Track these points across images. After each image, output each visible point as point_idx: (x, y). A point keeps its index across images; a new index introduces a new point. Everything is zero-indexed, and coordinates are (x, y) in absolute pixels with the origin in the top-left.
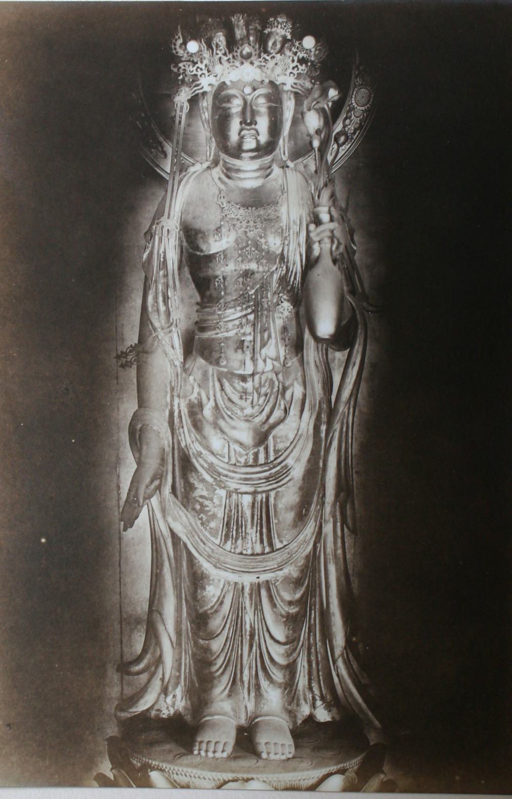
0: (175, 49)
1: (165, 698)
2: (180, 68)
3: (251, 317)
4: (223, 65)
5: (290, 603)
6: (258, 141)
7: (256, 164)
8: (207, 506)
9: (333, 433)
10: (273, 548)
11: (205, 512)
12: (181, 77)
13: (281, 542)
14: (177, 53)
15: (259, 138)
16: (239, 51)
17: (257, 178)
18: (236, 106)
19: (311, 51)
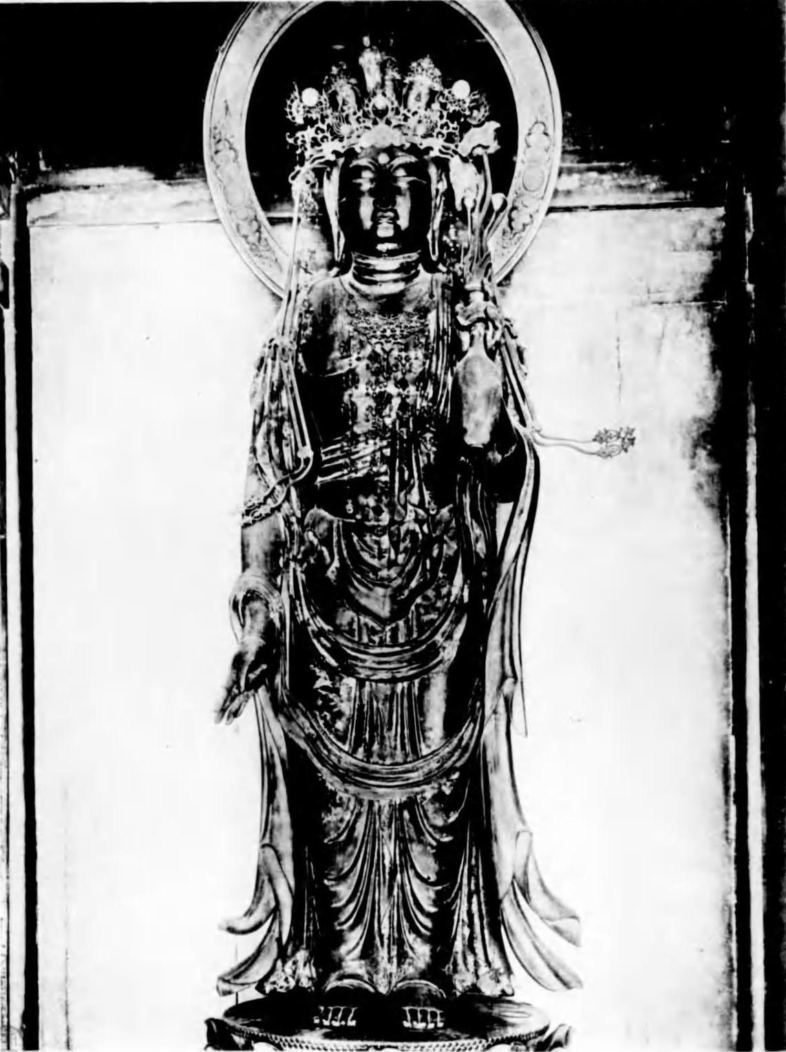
0: (291, 113)
1: (283, 966)
2: (297, 138)
3: (387, 452)
4: (351, 124)
5: (441, 830)
6: (397, 228)
7: (393, 263)
8: (332, 700)
9: (495, 604)
10: (417, 755)
11: (330, 709)
12: (299, 152)
13: (428, 747)
14: (294, 118)
15: (399, 222)
16: (371, 105)
17: (396, 281)
18: (366, 182)
19: (464, 103)
